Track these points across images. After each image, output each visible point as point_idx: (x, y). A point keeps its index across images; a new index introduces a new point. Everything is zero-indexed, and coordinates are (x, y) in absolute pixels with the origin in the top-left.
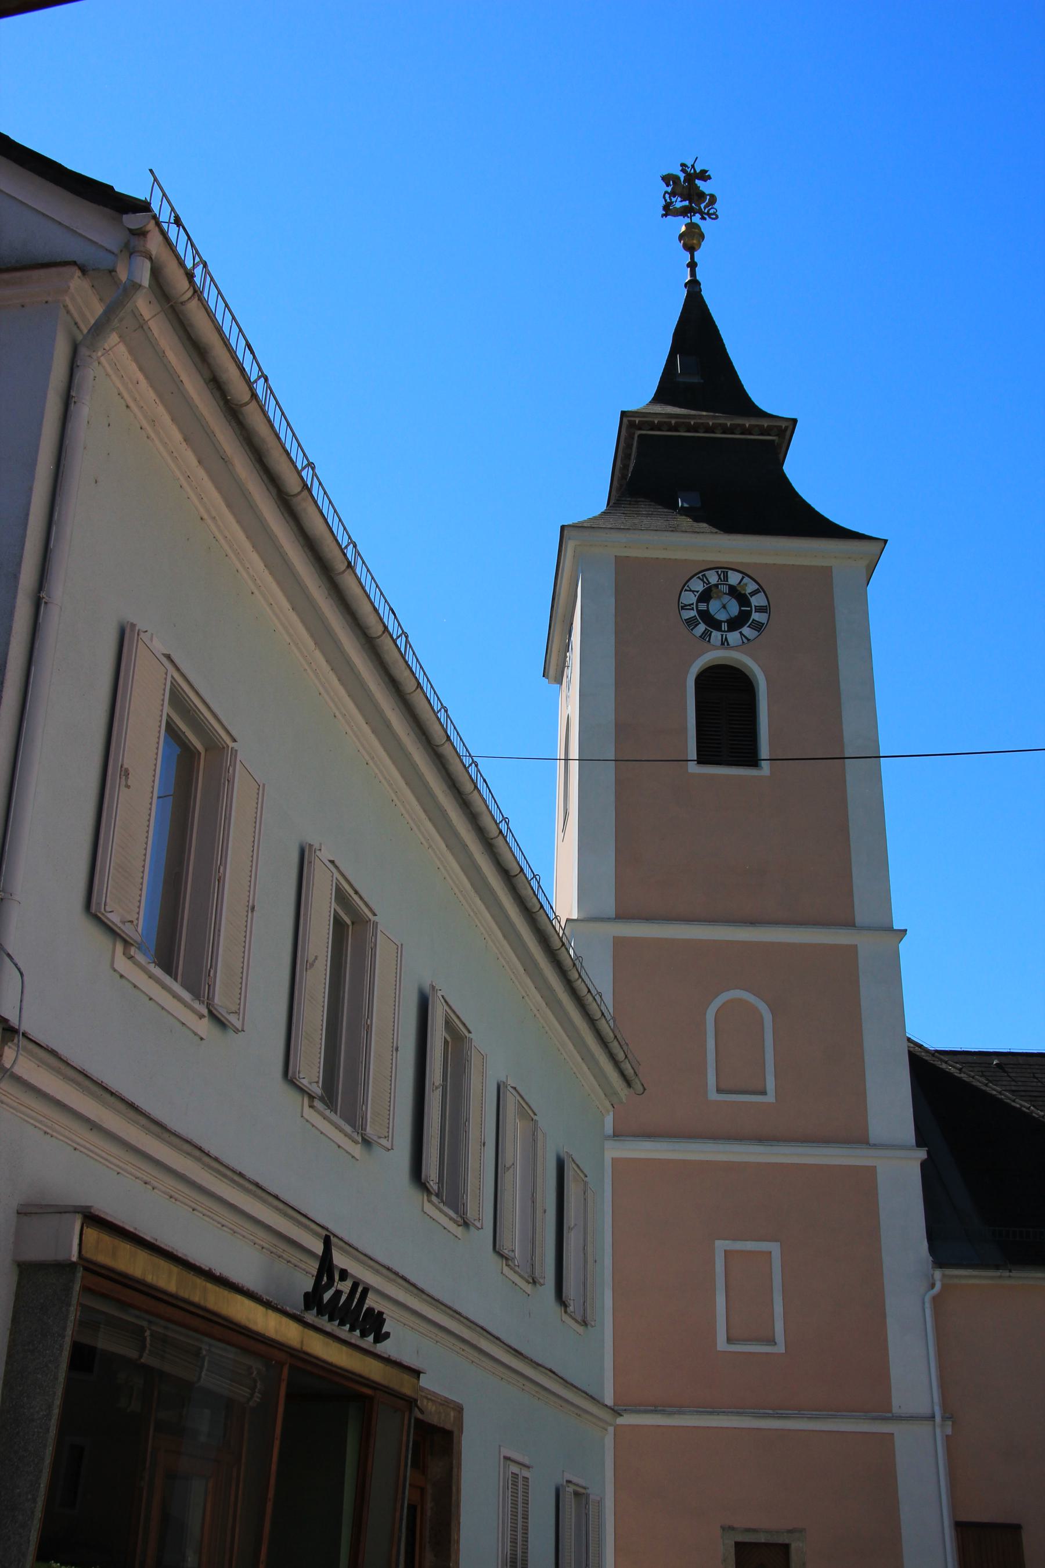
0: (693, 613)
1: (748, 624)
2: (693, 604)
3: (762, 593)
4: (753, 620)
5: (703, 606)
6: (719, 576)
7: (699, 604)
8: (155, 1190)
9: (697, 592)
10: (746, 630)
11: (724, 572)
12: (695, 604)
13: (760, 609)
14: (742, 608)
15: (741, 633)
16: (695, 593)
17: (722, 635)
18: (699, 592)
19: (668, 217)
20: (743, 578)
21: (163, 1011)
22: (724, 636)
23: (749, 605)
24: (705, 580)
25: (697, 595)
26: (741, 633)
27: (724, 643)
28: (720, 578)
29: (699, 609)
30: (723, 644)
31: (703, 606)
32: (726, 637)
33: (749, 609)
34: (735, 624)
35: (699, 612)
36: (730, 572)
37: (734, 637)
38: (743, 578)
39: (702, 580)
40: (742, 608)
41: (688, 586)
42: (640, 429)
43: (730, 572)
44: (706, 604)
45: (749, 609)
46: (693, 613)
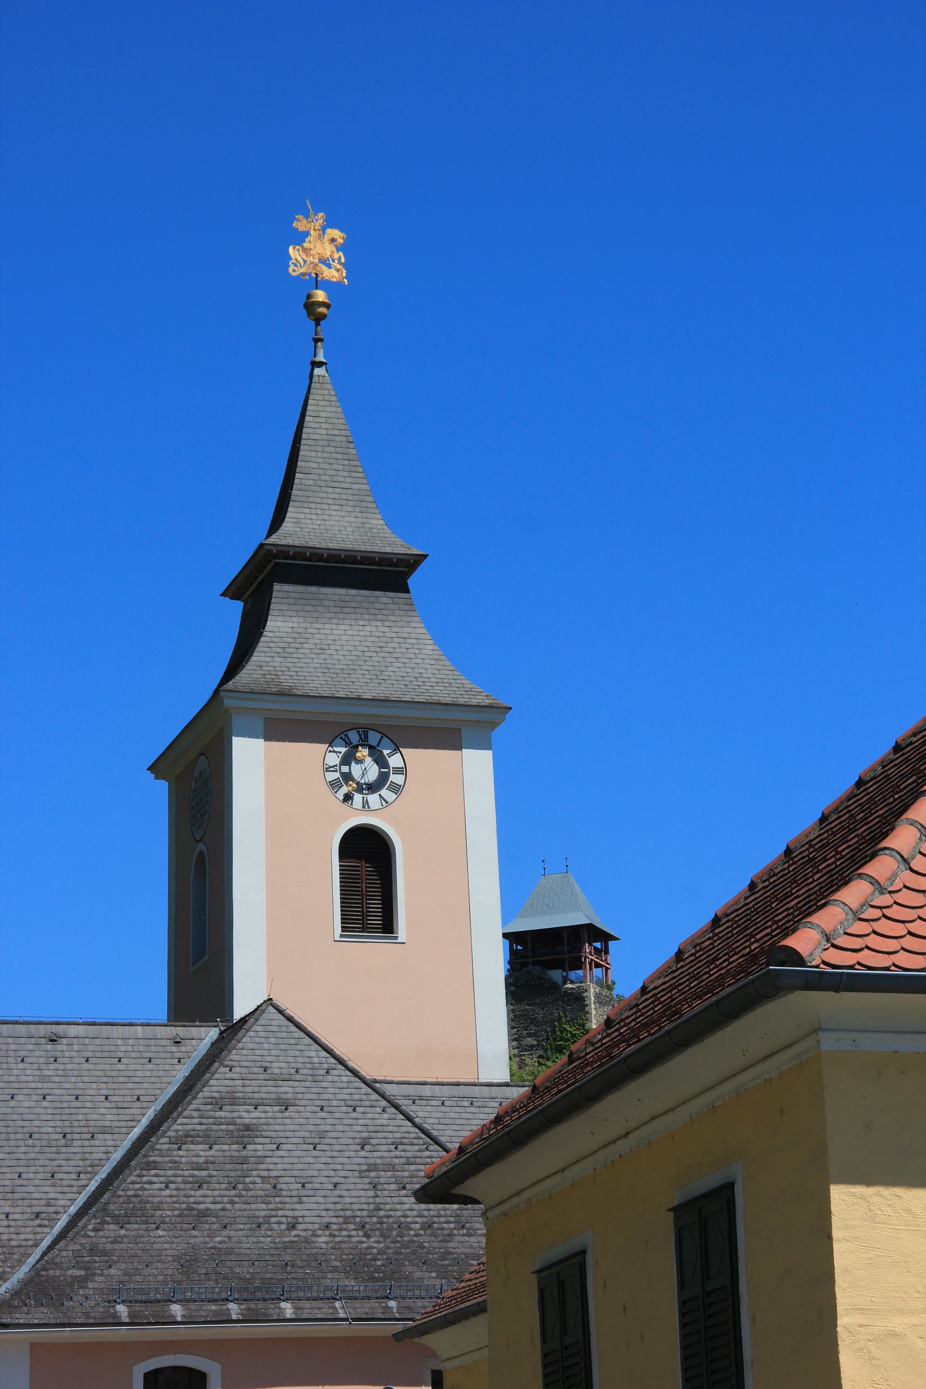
0: (337, 775)
1: (352, 745)
2: (336, 766)
3: (399, 754)
4: (391, 782)
5: (345, 769)
6: (360, 735)
7: (348, 771)
8: (764, 1080)
9: (340, 753)
10: (384, 792)
11: (364, 731)
12: (363, 796)
13: (398, 771)
14: (382, 770)
15: (380, 795)
16: (339, 754)
17: (363, 798)
18: (342, 753)
19: (412, 581)
20: (382, 737)
21: (676, 1110)
22: (365, 799)
23: (387, 766)
24: (347, 740)
25: (341, 756)
26: (380, 795)
27: (365, 804)
28: (361, 738)
29: (342, 771)
30: (364, 807)
31: (345, 769)
32: (367, 800)
33: (387, 770)
34: (372, 788)
35: (343, 774)
36: (370, 732)
37: (373, 799)
38: (382, 737)
39: (345, 740)
40: (382, 770)
41: (382, 805)
42: (277, 558)
43: (370, 732)
44: (348, 767)
45: (387, 770)
46: (337, 775)
